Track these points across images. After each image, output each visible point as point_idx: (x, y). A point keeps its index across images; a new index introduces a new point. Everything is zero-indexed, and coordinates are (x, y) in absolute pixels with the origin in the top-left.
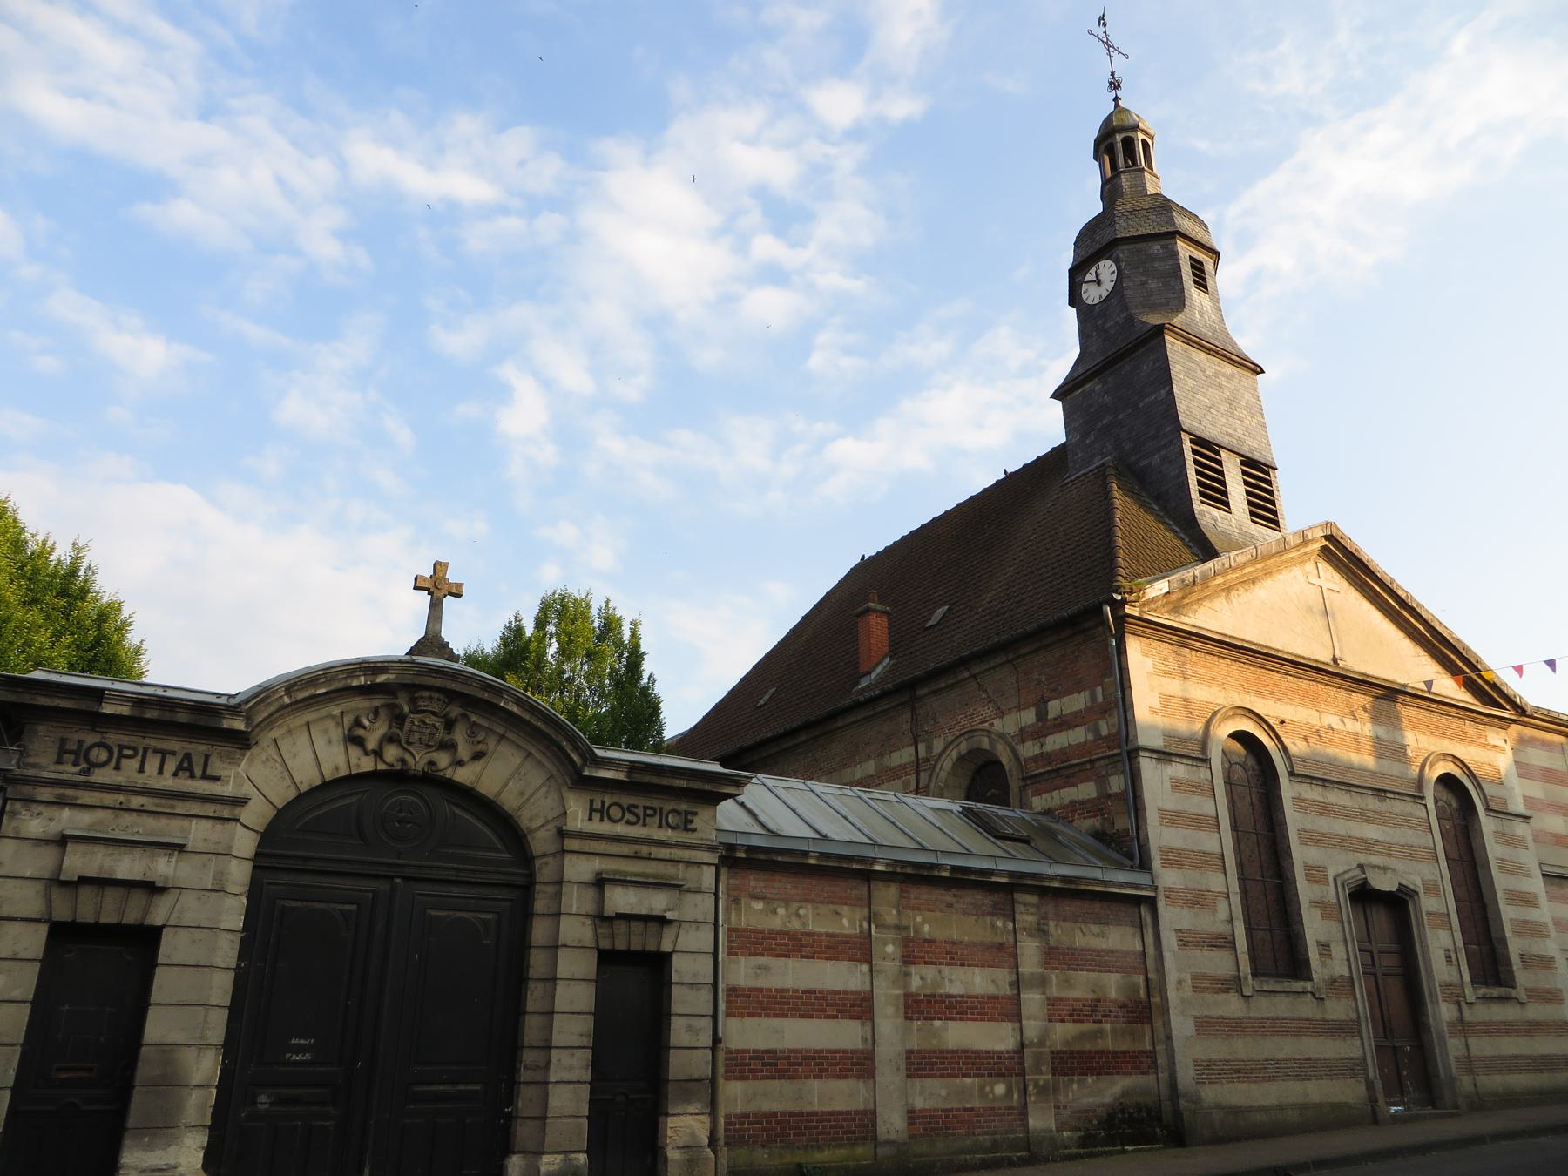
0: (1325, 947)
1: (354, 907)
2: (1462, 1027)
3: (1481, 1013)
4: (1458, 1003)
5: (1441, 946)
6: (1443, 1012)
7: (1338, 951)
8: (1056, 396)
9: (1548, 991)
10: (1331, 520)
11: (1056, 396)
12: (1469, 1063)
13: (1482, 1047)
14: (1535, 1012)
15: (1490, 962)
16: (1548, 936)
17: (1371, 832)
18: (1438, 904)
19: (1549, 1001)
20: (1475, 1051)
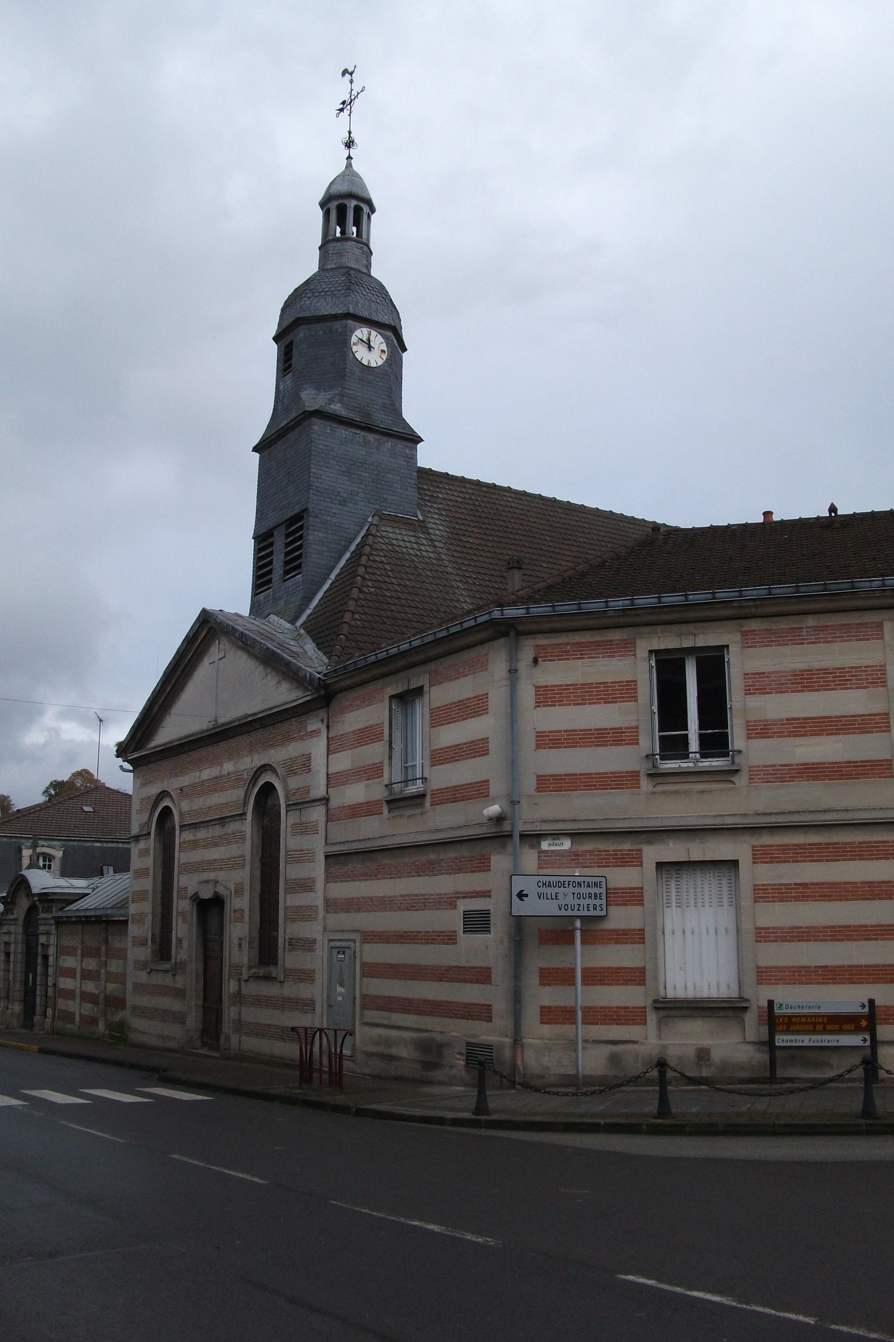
0: (180, 941)
1: (338, 235)
2: (239, 998)
3: (254, 989)
4: (240, 980)
5: (238, 931)
6: (231, 987)
7: (185, 944)
8: (255, 449)
9: (303, 972)
10: (320, 195)
11: (255, 449)
12: (239, 1025)
13: (250, 1015)
14: (291, 990)
15: (267, 949)
16: (316, 919)
17: (214, 854)
18: (242, 903)
19: (302, 980)
20: (244, 991)
